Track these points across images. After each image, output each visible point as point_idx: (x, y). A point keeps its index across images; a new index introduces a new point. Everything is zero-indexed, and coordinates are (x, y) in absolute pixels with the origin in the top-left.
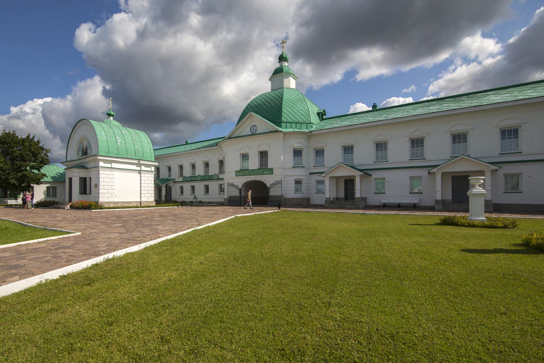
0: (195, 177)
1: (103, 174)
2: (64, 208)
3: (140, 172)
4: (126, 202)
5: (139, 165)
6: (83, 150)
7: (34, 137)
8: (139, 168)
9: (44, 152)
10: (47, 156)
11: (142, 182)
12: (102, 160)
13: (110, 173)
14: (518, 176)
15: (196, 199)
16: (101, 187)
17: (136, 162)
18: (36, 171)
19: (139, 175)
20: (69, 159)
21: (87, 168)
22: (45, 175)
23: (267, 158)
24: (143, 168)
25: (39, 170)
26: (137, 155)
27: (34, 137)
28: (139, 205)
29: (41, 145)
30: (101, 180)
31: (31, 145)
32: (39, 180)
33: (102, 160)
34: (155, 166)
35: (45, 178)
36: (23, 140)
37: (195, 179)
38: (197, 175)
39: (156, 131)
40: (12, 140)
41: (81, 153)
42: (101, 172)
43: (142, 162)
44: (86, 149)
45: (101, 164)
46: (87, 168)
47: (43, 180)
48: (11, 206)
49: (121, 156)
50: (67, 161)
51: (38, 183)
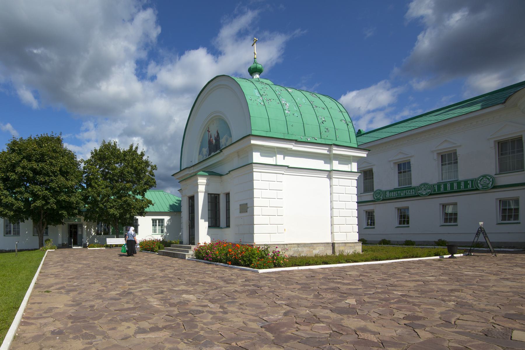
0: (411, 188)
1: (260, 179)
2: (183, 257)
3: (330, 173)
4: (305, 245)
5: (328, 158)
6: (210, 142)
7: (137, 148)
8: (327, 167)
9: (149, 169)
10: (153, 175)
11: (335, 197)
12: (259, 148)
13: (273, 177)
14: (407, 208)
15: (485, 235)
16: (256, 211)
17: (324, 151)
18: (139, 197)
19: (328, 180)
20: (182, 169)
21: (221, 175)
22: (150, 202)
23: (373, 178)
24: (336, 165)
25: (143, 195)
26: (324, 135)
27: (137, 148)
28: (329, 252)
29: (144, 158)
30: (256, 193)
31: (134, 159)
32: (143, 208)
33: (259, 148)
34: (358, 160)
35: (151, 206)
36: (125, 153)
37: (412, 193)
38: (415, 183)
39: (360, 83)
40: (112, 153)
41: (205, 150)
42: (256, 176)
43: (336, 151)
44: (218, 139)
45: (257, 157)
46: (221, 175)
47: (147, 210)
48: (111, 246)
49: (293, 140)
50: (181, 171)
51: (142, 213)
